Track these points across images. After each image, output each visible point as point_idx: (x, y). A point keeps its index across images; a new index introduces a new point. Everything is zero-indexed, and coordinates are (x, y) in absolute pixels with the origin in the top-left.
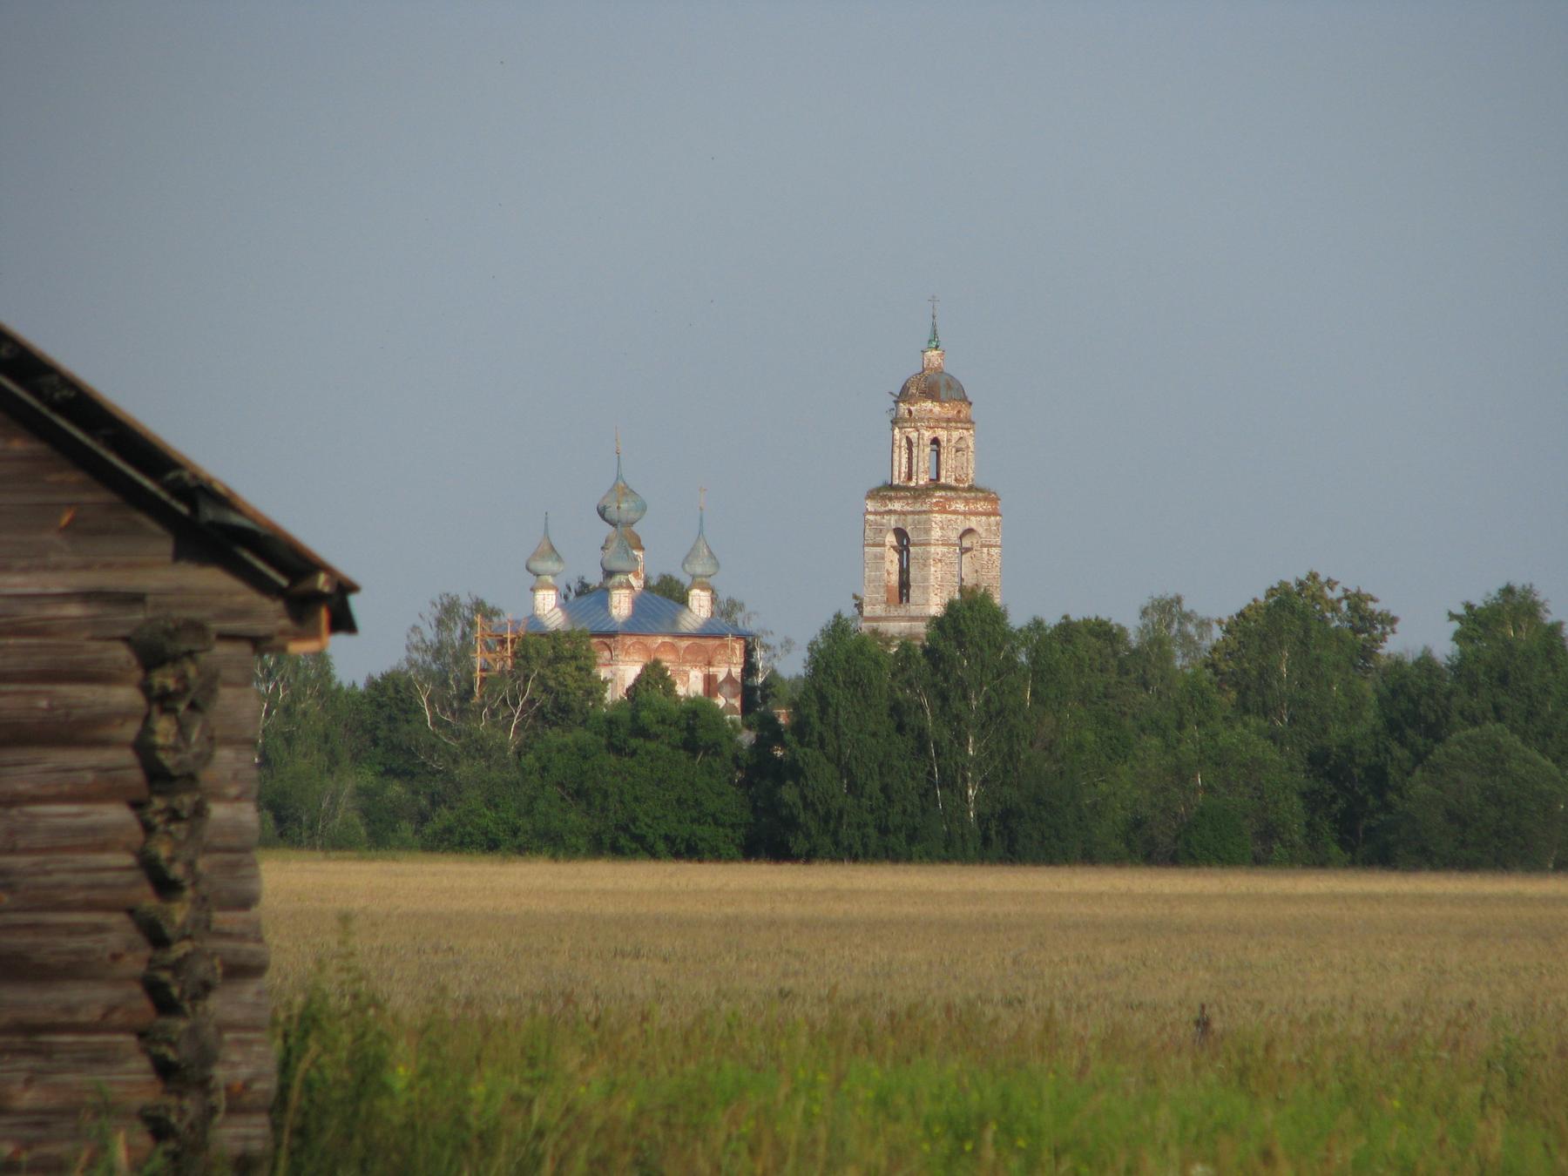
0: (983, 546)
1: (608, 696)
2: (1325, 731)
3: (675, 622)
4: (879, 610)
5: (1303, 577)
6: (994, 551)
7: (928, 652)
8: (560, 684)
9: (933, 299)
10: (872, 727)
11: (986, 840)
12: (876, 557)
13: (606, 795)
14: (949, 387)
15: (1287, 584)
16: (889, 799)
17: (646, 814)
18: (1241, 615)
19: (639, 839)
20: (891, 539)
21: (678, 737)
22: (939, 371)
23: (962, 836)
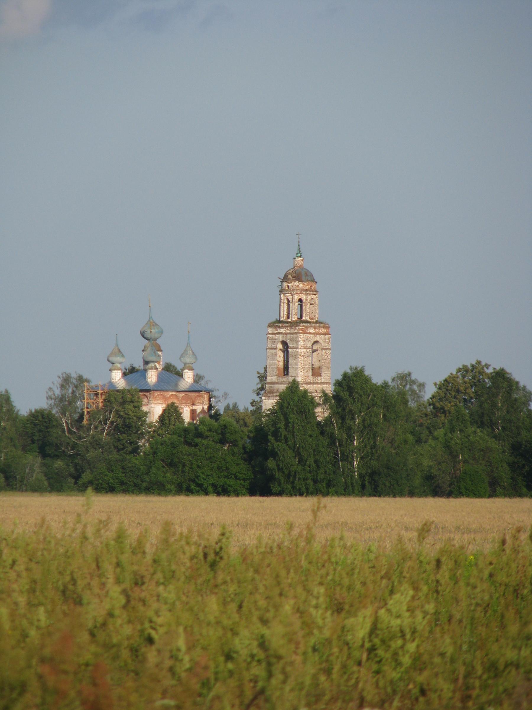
0: (323, 349)
1: (148, 420)
2: (519, 434)
3: (177, 385)
4: (274, 379)
5: (474, 363)
6: (327, 351)
7: (334, 397)
8: (126, 414)
9: (298, 234)
10: (310, 432)
11: (363, 487)
12: (272, 354)
13: (184, 466)
14: (306, 275)
15: (466, 366)
16: (318, 466)
17: (203, 473)
18: (446, 380)
19: (200, 486)
20: (280, 346)
21: (217, 437)
22: (301, 267)
23: (352, 484)
